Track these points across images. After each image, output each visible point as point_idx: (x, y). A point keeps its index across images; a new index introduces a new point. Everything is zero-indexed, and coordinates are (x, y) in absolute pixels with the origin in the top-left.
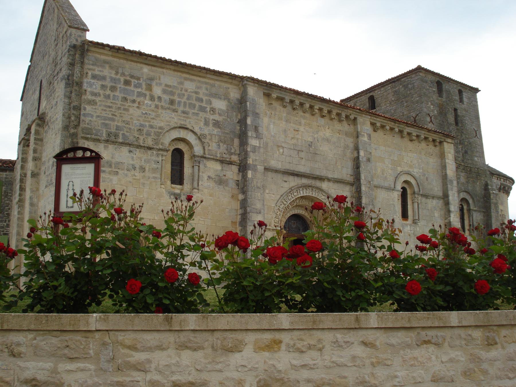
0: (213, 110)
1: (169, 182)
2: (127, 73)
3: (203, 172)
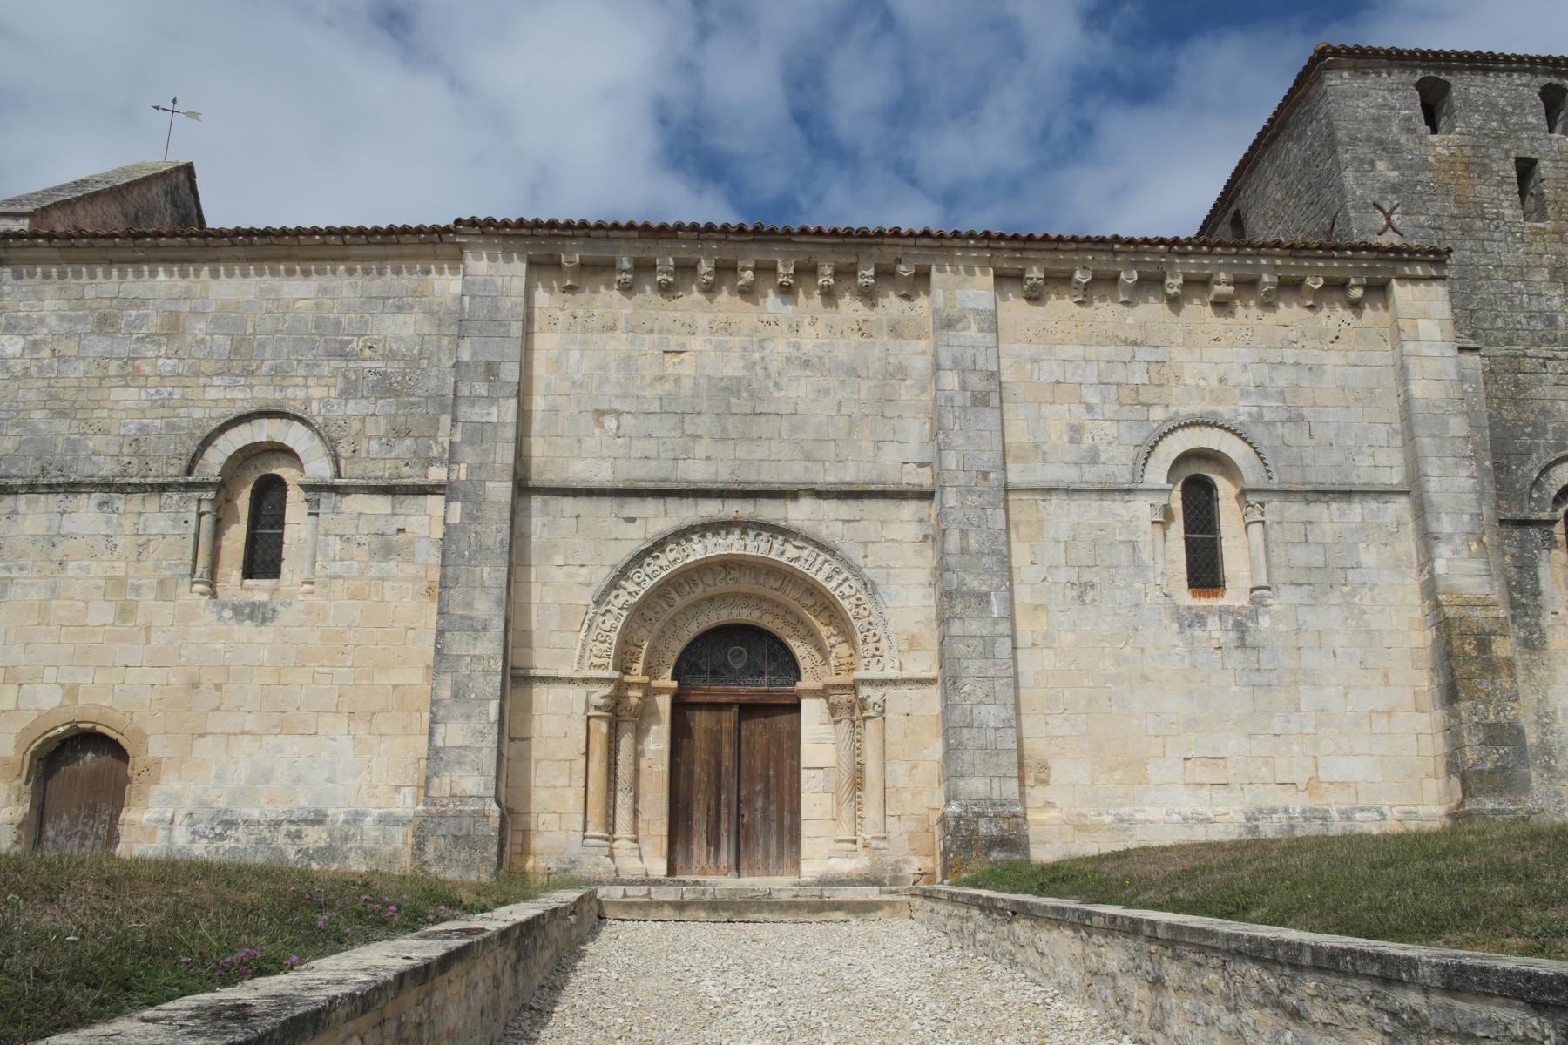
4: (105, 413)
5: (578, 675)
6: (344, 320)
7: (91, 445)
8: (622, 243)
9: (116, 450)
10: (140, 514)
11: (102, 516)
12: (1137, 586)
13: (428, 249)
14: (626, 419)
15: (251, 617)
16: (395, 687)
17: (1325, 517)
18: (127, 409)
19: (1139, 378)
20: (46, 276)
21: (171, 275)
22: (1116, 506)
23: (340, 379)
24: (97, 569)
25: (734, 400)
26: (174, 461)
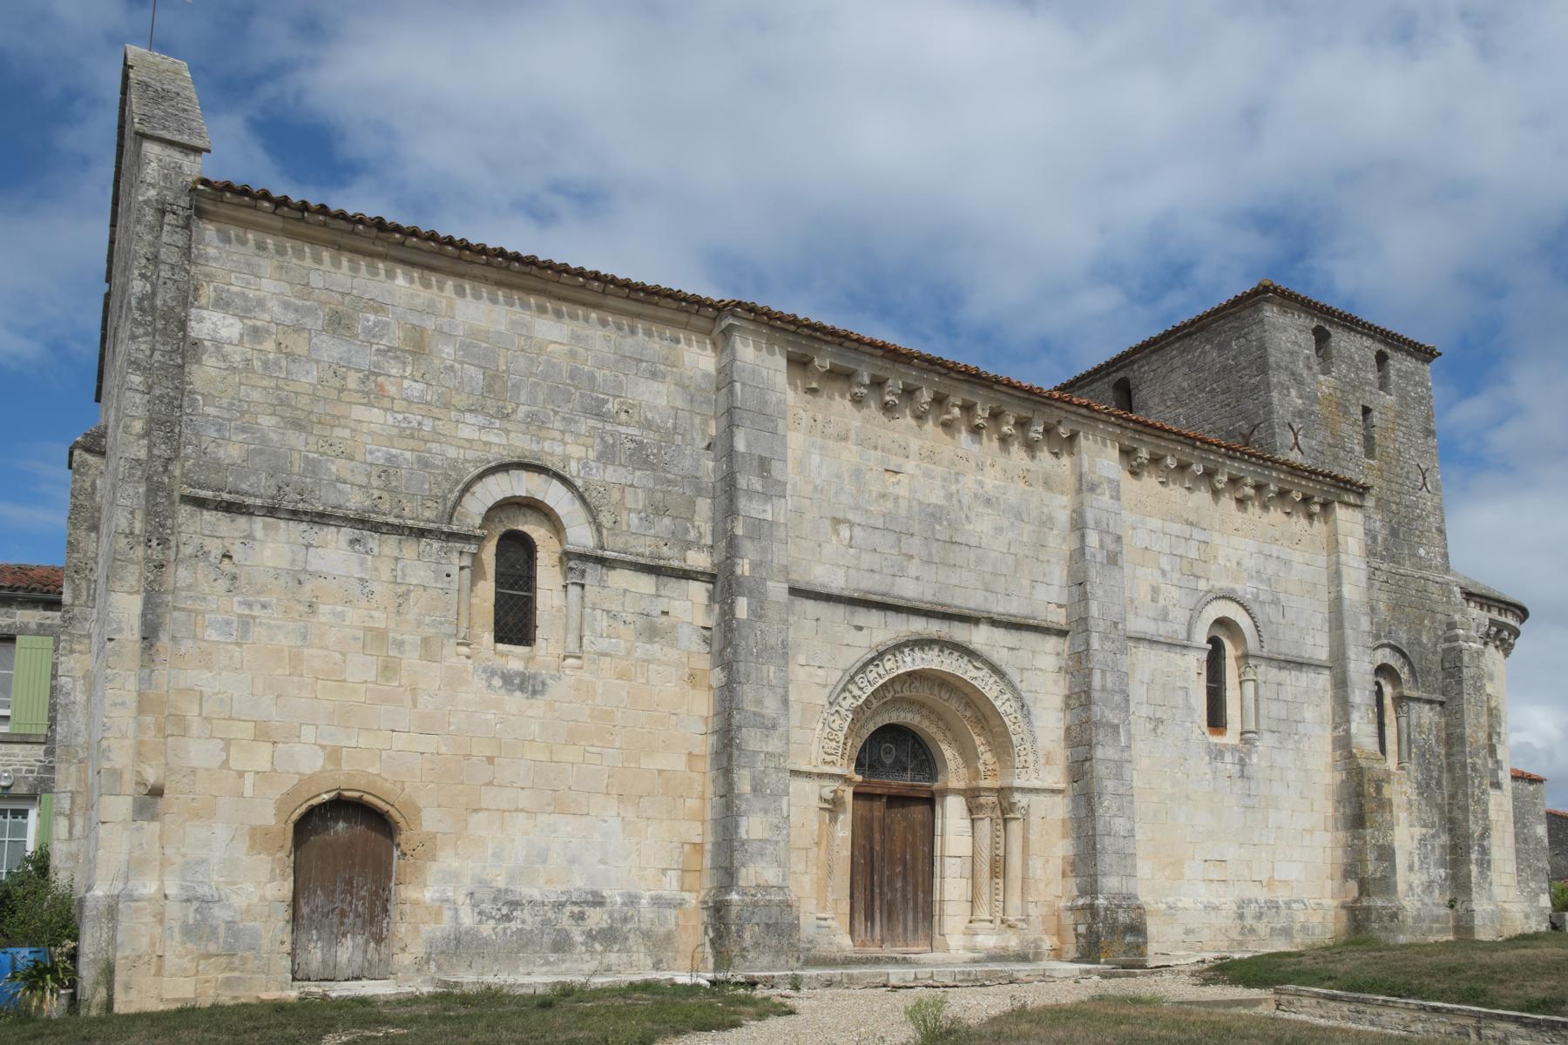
4: (346, 433)
5: (815, 770)
6: (599, 375)
7: (334, 469)
8: (867, 358)
9: (363, 480)
10: (397, 559)
11: (354, 556)
13: (683, 317)
14: (857, 531)
15: (522, 688)
16: (660, 771)
18: (372, 433)
19: (1193, 554)
20: (261, 247)
21: (412, 281)
22: (1176, 657)
23: (598, 441)
24: (353, 616)
25: (938, 527)
26: (430, 504)
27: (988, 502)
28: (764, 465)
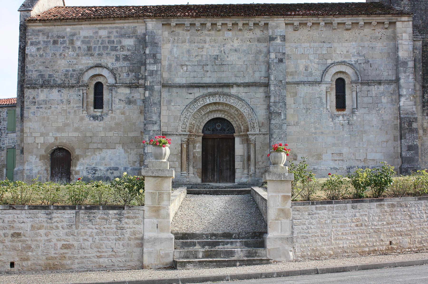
0: (123, 47)
1: (92, 108)
2: (55, 35)
3: (114, 97)
12: (322, 109)
13: (136, 21)
17: (373, 89)
24: (59, 107)
25: (216, 61)
27: (236, 50)
28: (154, 56)
